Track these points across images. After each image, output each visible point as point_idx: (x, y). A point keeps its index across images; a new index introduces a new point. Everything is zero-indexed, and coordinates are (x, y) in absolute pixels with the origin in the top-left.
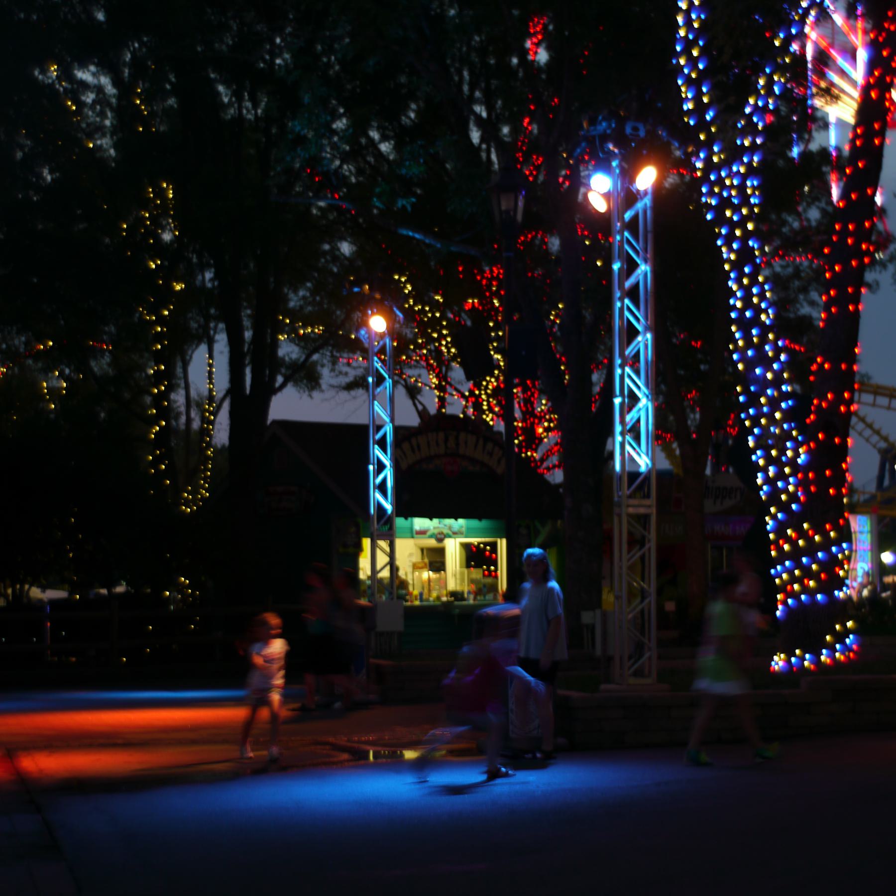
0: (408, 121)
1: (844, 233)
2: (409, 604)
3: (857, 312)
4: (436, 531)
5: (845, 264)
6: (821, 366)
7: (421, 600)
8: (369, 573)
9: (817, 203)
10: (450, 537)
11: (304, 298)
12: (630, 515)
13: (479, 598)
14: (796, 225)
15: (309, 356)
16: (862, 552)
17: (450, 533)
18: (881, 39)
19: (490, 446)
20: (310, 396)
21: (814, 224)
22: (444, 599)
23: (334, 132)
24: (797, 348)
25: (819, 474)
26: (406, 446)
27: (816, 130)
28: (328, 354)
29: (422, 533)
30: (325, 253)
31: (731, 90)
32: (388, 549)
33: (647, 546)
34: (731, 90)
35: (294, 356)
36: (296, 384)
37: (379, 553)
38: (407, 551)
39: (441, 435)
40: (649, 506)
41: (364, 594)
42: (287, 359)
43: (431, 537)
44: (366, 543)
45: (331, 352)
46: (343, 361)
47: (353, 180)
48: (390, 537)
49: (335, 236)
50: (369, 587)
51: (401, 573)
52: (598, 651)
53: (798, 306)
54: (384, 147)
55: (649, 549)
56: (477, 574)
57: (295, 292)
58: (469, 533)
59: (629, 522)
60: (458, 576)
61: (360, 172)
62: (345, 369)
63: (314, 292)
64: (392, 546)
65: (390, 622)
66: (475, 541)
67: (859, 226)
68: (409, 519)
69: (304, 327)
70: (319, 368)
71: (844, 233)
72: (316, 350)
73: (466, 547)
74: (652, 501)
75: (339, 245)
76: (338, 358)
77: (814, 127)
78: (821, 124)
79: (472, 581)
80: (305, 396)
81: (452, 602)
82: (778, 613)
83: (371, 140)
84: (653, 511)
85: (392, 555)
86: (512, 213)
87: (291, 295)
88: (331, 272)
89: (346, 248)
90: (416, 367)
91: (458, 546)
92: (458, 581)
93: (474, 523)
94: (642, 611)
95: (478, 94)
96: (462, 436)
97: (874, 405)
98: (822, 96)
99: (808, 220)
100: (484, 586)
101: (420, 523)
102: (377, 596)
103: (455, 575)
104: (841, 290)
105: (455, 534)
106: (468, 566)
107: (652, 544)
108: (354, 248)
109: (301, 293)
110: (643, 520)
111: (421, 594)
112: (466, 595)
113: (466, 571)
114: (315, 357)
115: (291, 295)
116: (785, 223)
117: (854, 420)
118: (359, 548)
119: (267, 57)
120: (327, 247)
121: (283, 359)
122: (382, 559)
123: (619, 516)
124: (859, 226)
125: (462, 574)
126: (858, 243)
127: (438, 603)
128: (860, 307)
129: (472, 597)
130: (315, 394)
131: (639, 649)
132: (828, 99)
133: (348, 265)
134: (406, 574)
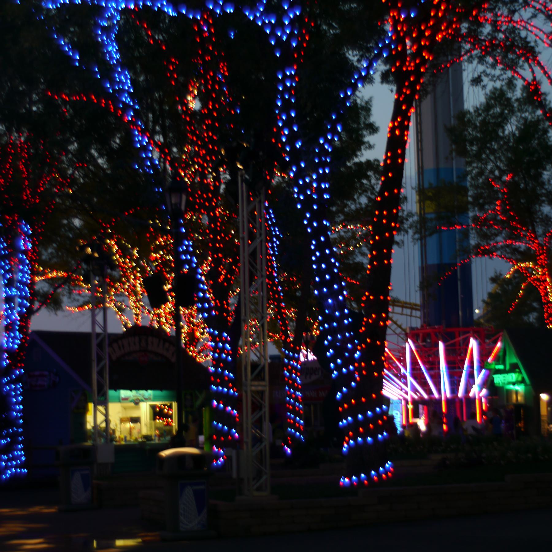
0: (141, 50)
1: (381, 217)
2: (118, 443)
3: (389, 263)
4: (134, 398)
5: (382, 236)
6: (368, 297)
7: (126, 441)
8: (92, 424)
9: (365, 194)
10: (143, 401)
11: (52, 253)
12: (252, 391)
13: (161, 439)
14: (353, 207)
15: (55, 290)
16: (397, 404)
17: (143, 399)
18: (401, 99)
19: (167, 345)
20: (56, 314)
21: (364, 206)
22: (140, 440)
23: (69, 151)
24: (354, 282)
25: (368, 364)
26: (115, 346)
27: (364, 149)
28: (67, 288)
29: (126, 399)
30: (64, 225)
31: (311, 130)
32: (104, 411)
33: (263, 410)
34: (311, 130)
35: (46, 289)
36: (47, 307)
37: (99, 414)
38: (116, 410)
39: (137, 339)
40: (265, 386)
41: (90, 438)
42: (41, 291)
43: (131, 401)
44: (91, 406)
45: (69, 287)
46: (75, 292)
47: (82, 181)
48: (104, 402)
49: (69, 215)
50: (93, 433)
51: (112, 426)
52: (234, 475)
53: (355, 256)
54: (100, 161)
55: (265, 413)
56: (159, 422)
57: (46, 250)
58: (155, 398)
59: (253, 396)
60: (148, 425)
61: (85, 176)
62: (77, 297)
63: (57, 250)
64: (106, 409)
65: (105, 457)
66: (158, 403)
67: (390, 212)
68: (118, 391)
69: (51, 272)
70: (61, 297)
71: (381, 217)
72: (59, 286)
73: (153, 407)
74: (266, 383)
75: (73, 220)
76: (72, 290)
77: (362, 147)
78: (367, 145)
79: (157, 428)
80: (52, 314)
81: (145, 442)
82: (344, 449)
83: (92, 156)
84: (267, 389)
85: (106, 415)
86: (178, 205)
87: (43, 252)
88: (68, 237)
89: (77, 222)
90: (121, 295)
91: (148, 407)
92: (149, 429)
93: (158, 393)
94: (261, 451)
95: (158, 128)
96: (150, 339)
97: (402, 314)
98: (367, 129)
99: (360, 204)
100: (165, 431)
101: (124, 393)
102: (98, 439)
103: (146, 426)
104: (379, 251)
105: (146, 399)
106: (155, 419)
107: (266, 409)
108: (82, 222)
109: (50, 250)
110: (262, 393)
111: (125, 437)
112: (153, 437)
113: (153, 422)
114: (59, 290)
115: (43, 252)
116: (346, 206)
117: (389, 331)
118: (85, 410)
119: (28, 106)
120: (65, 222)
121: (39, 291)
122: (101, 418)
123: (246, 392)
124: (390, 212)
125: (151, 424)
126: (389, 223)
127: (136, 443)
128: (391, 261)
129: (157, 438)
130: (59, 313)
131: (259, 474)
132: (371, 130)
133: (79, 233)
134: (116, 425)
